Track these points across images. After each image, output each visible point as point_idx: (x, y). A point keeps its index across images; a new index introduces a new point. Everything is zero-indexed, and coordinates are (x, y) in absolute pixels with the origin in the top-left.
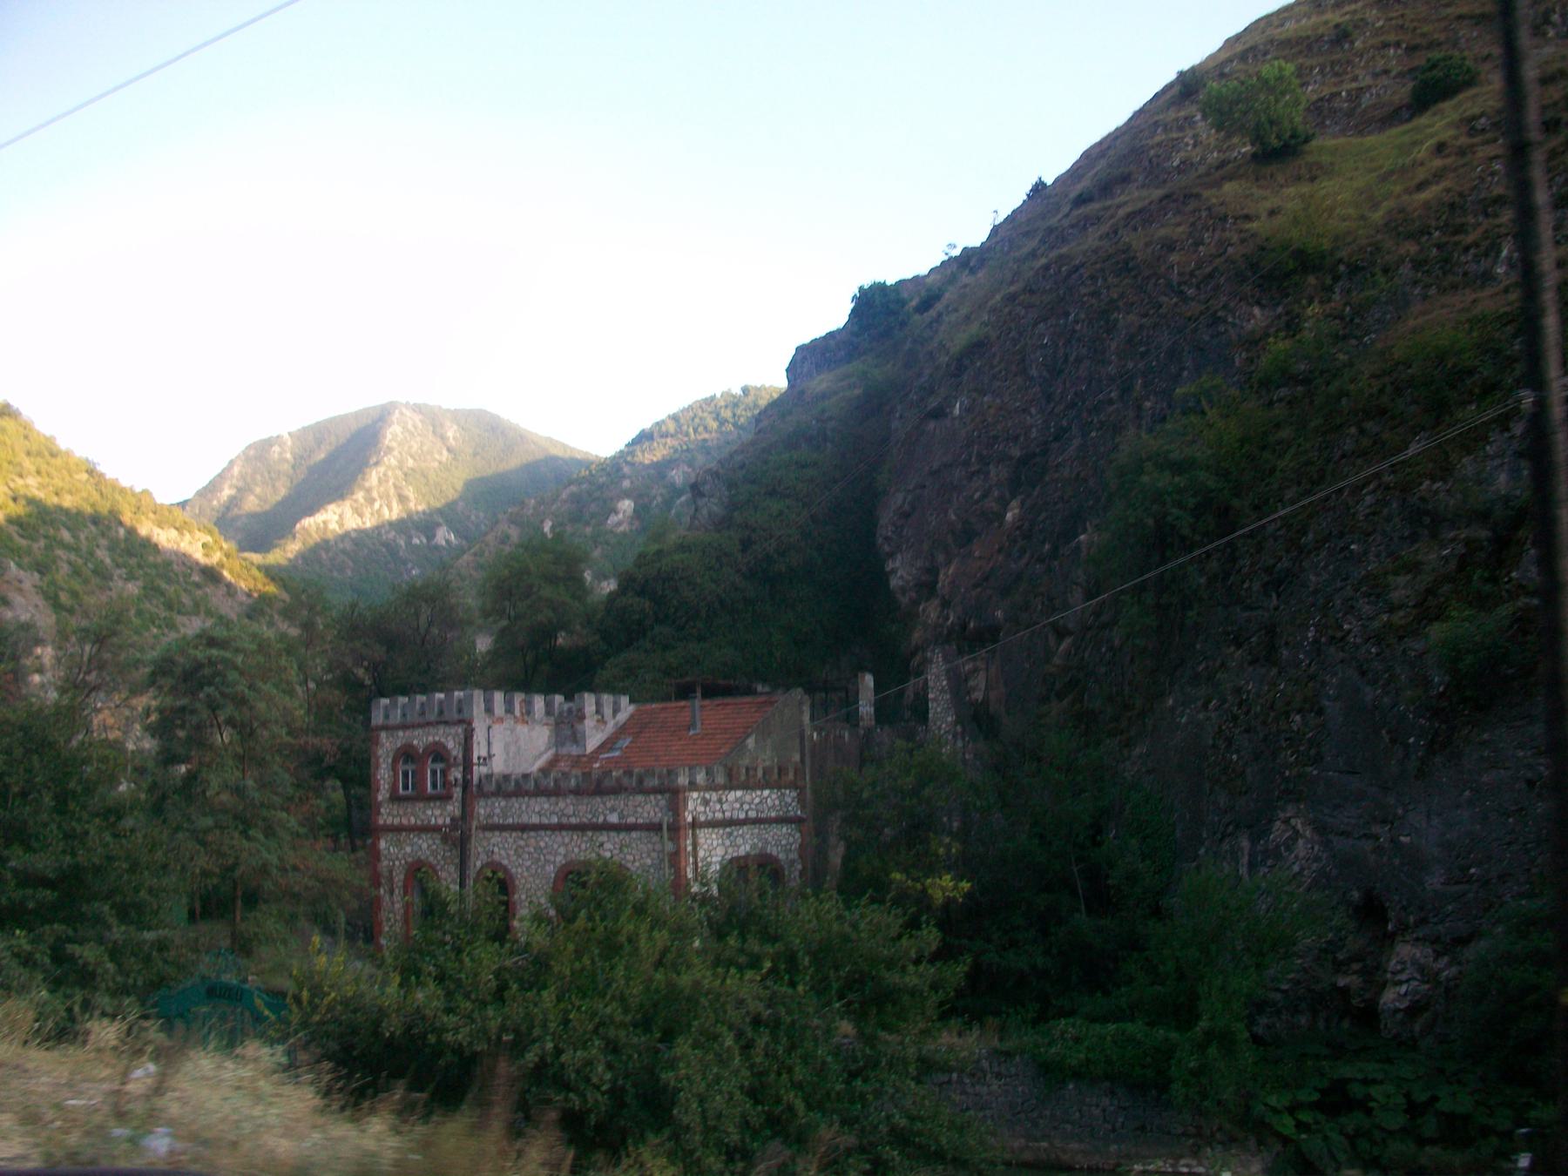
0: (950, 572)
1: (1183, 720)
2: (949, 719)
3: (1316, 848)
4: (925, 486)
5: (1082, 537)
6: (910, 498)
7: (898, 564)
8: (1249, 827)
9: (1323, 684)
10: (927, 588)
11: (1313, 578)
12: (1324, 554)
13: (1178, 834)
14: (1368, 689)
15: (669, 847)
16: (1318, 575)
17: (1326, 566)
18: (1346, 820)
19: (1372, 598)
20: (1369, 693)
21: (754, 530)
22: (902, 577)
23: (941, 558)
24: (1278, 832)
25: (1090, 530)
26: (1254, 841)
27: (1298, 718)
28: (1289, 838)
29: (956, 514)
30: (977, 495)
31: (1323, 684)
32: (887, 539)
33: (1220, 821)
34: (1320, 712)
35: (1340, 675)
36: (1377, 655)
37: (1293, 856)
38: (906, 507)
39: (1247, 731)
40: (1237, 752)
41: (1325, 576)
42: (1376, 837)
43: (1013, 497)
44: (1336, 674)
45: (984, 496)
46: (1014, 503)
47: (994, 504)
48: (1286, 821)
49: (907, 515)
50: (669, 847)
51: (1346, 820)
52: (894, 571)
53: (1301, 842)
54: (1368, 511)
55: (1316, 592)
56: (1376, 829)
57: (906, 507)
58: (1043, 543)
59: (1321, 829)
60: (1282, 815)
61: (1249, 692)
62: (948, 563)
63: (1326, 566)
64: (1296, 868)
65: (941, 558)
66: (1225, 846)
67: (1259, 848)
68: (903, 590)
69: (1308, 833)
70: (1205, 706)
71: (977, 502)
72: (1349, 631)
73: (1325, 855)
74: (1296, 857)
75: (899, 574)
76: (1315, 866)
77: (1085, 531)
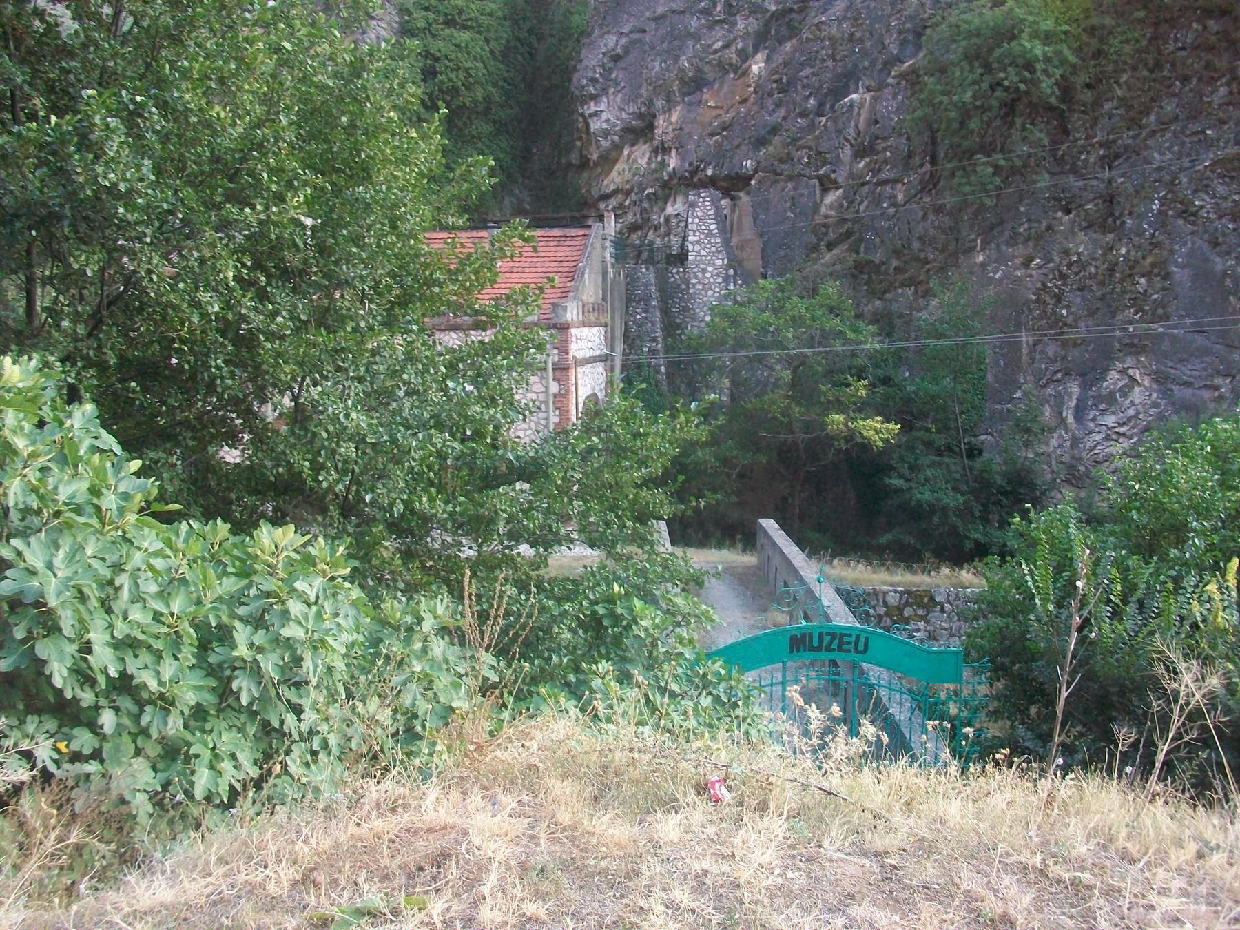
0: (674, 118)
1: (997, 276)
2: (719, 262)
3: (1154, 396)
4: (645, 31)
5: (854, 96)
6: (623, 41)
7: (603, 107)
8: (1081, 375)
9: (1172, 252)
10: (641, 130)
11: (1156, 155)
12: (1169, 135)
13: (990, 378)
14: (1218, 260)
15: (554, 388)
16: (1161, 154)
17: (1171, 146)
18: (1189, 373)
19: (1226, 180)
20: (1219, 264)
21: (437, 60)
22: (607, 121)
23: (659, 103)
24: (1113, 379)
25: (861, 90)
26: (1085, 386)
27: (1143, 281)
28: (1125, 386)
29: (689, 62)
30: (718, 45)
31: (1172, 252)
32: (593, 81)
33: (1047, 369)
34: (1167, 276)
35: (1189, 245)
36: (1234, 230)
37: (1128, 401)
38: (619, 50)
39: (1081, 289)
40: (1067, 307)
41: (1169, 156)
42: (1217, 388)
43: (756, 51)
44: (1185, 244)
45: (726, 46)
46: (760, 57)
47: (734, 56)
48: (1123, 372)
49: (616, 59)
50: (554, 388)
51: (1189, 373)
52: (597, 114)
53: (1137, 389)
54: (1221, 101)
55: (1159, 169)
56: (1218, 381)
57: (619, 50)
58: (807, 98)
59: (1160, 379)
60: (1119, 366)
61: (1079, 254)
62: (668, 110)
63: (1171, 146)
64: (1131, 412)
65: (659, 103)
66: (1050, 391)
67: (1091, 393)
68: (606, 134)
69: (1146, 383)
70: (1027, 264)
71: (716, 52)
72: (1202, 207)
73: (1163, 402)
74: (1132, 403)
75: (604, 116)
76: (1152, 411)
77: (856, 91)
